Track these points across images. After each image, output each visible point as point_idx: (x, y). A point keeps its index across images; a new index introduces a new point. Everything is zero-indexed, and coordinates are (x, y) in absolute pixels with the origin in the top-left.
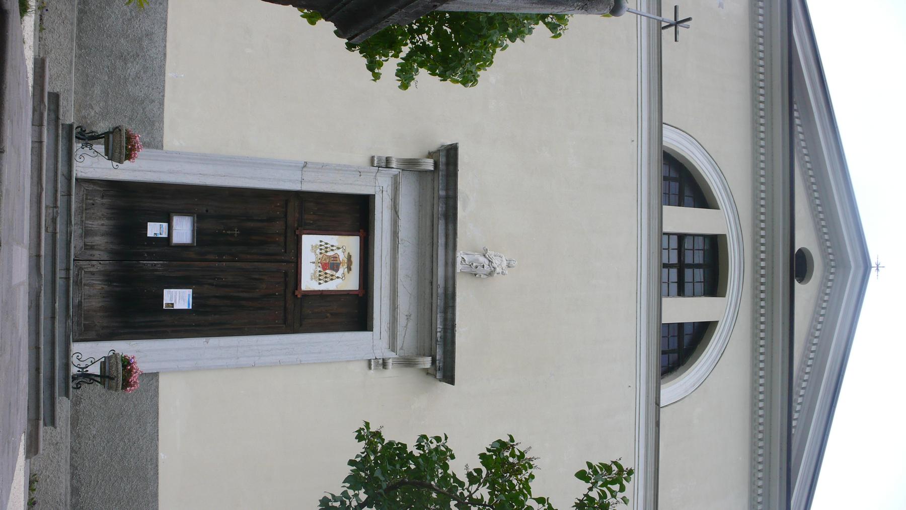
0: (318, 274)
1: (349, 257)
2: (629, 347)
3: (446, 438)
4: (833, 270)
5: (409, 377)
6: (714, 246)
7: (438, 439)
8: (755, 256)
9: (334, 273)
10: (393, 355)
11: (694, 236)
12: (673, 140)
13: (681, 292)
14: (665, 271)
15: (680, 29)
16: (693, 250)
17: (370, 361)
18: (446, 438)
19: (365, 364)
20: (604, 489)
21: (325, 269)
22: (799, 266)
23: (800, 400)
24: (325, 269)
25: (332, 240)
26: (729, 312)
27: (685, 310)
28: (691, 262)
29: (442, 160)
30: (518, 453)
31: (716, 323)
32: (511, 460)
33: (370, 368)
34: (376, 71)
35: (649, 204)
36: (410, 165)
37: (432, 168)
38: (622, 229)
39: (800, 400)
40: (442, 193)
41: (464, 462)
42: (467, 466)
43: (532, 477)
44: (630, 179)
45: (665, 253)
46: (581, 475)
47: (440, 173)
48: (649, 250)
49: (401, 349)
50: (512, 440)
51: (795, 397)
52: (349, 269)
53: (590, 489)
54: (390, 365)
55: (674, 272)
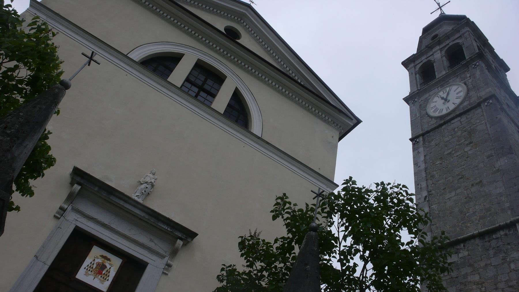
0: (102, 279)
1: (102, 256)
2: (225, 134)
3: (224, 265)
4: (242, 21)
5: (182, 255)
6: (200, 67)
7: (223, 269)
8: (216, 51)
9: (106, 269)
10: (167, 258)
11: (190, 73)
12: (137, 55)
13: (214, 96)
14: (199, 97)
15: (94, 58)
16: (197, 78)
17: (163, 273)
18: (224, 265)
19: (164, 276)
20: (286, 211)
21: (101, 274)
22: (232, 35)
23: (291, 72)
24: (101, 274)
25: (88, 261)
26: (236, 80)
27: (222, 100)
28: (202, 82)
29: (78, 179)
30: (250, 238)
31: (236, 88)
32: (251, 243)
33: (167, 274)
34: (14, 207)
35: (163, 86)
36: (71, 198)
37: (80, 187)
38: (165, 107)
39: (291, 72)
40: (96, 189)
41: (241, 265)
42: (243, 266)
43: (263, 241)
44: (145, 89)
45: (190, 92)
46: (274, 218)
47: (83, 181)
48: (185, 100)
49: (166, 252)
50: (242, 237)
51: (288, 73)
52: (109, 260)
53: (283, 217)
54: (171, 263)
55: (202, 94)
